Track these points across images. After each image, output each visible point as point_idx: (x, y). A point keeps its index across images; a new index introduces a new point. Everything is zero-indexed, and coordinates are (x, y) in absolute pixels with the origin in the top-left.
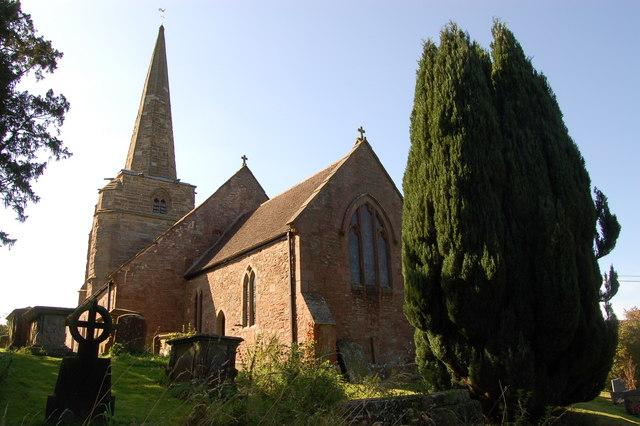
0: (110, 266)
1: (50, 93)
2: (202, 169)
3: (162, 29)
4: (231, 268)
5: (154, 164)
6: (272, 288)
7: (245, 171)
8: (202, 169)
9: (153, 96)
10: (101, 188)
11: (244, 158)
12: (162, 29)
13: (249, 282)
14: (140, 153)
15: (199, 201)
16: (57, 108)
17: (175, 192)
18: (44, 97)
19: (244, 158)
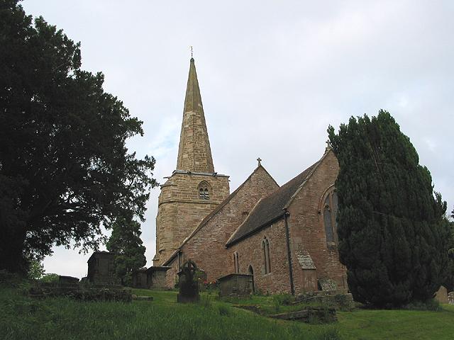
0: (173, 241)
1: (146, 157)
2: (233, 167)
3: (192, 61)
4: (255, 238)
5: (197, 163)
6: (279, 249)
7: (260, 166)
8: (233, 167)
9: (191, 113)
10: (46, 19)
11: (259, 160)
12: (192, 61)
13: (266, 244)
14: (185, 156)
15: (233, 187)
16: (61, 31)
17: (213, 183)
18: (144, 160)
19: (259, 160)
